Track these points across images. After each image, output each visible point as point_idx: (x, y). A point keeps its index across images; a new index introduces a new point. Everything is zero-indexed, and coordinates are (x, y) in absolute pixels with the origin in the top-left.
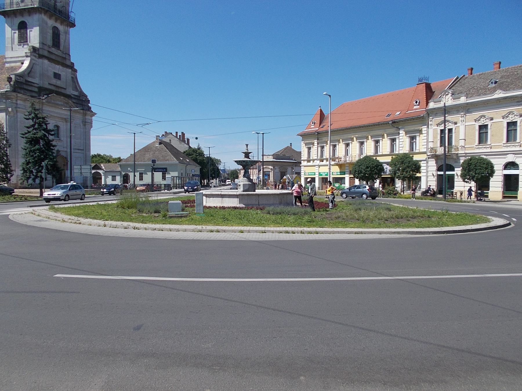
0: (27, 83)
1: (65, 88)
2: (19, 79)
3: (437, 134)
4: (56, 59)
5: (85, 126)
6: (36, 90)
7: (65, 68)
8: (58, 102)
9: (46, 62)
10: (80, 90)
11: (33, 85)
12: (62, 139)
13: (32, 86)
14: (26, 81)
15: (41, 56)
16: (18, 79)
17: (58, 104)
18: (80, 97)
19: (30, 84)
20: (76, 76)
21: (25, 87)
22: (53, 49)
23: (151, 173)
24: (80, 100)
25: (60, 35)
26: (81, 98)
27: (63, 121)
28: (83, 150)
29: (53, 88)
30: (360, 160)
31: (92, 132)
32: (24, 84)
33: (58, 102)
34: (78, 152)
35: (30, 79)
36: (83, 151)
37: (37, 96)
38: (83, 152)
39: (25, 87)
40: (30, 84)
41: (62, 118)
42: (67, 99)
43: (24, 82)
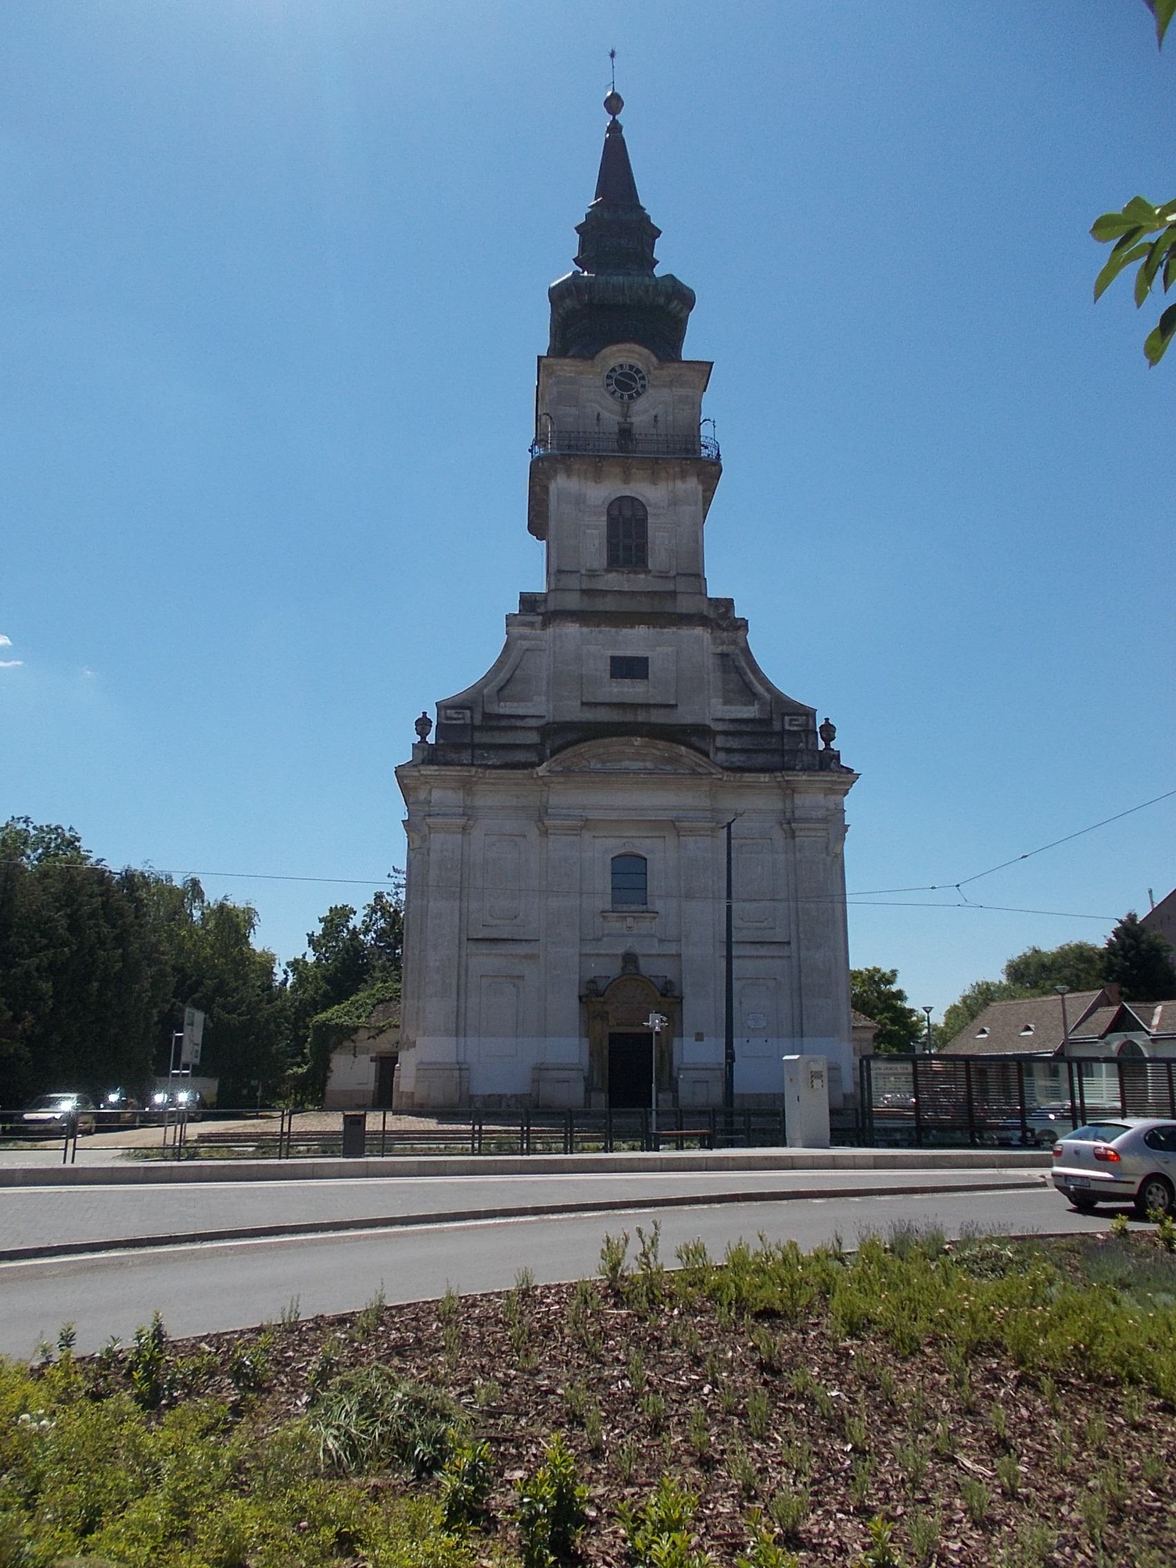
0: (493, 722)
1: (672, 702)
2: (455, 716)
3: (608, 1216)
4: (623, 609)
5: (793, 837)
6: (533, 738)
7: (669, 631)
8: (626, 764)
9: (572, 630)
10: (767, 696)
11: (519, 723)
12: (658, 905)
13: (516, 728)
14: (487, 716)
15: (553, 617)
16: (451, 719)
17: (626, 772)
18: (767, 722)
19: (504, 723)
20: (743, 645)
21: (480, 738)
22: (612, 576)
23: (735, 1091)
24: (773, 734)
25: (645, 520)
26: (777, 726)
27: (662, 834)
28: (789, 943)
29: (603, 715)
30: (1154, 910)
31: (851, 849)
32: (480, 728)
33: (626, 764)
34: (754, 953)
35: (506, 708)
36: (786, 947)
37: (535, 759)
38: (785, 951)
39: (480, 738)
40: (504, 723)
41: (656, 825)
42: (662, 744)
43: (478, 720)
